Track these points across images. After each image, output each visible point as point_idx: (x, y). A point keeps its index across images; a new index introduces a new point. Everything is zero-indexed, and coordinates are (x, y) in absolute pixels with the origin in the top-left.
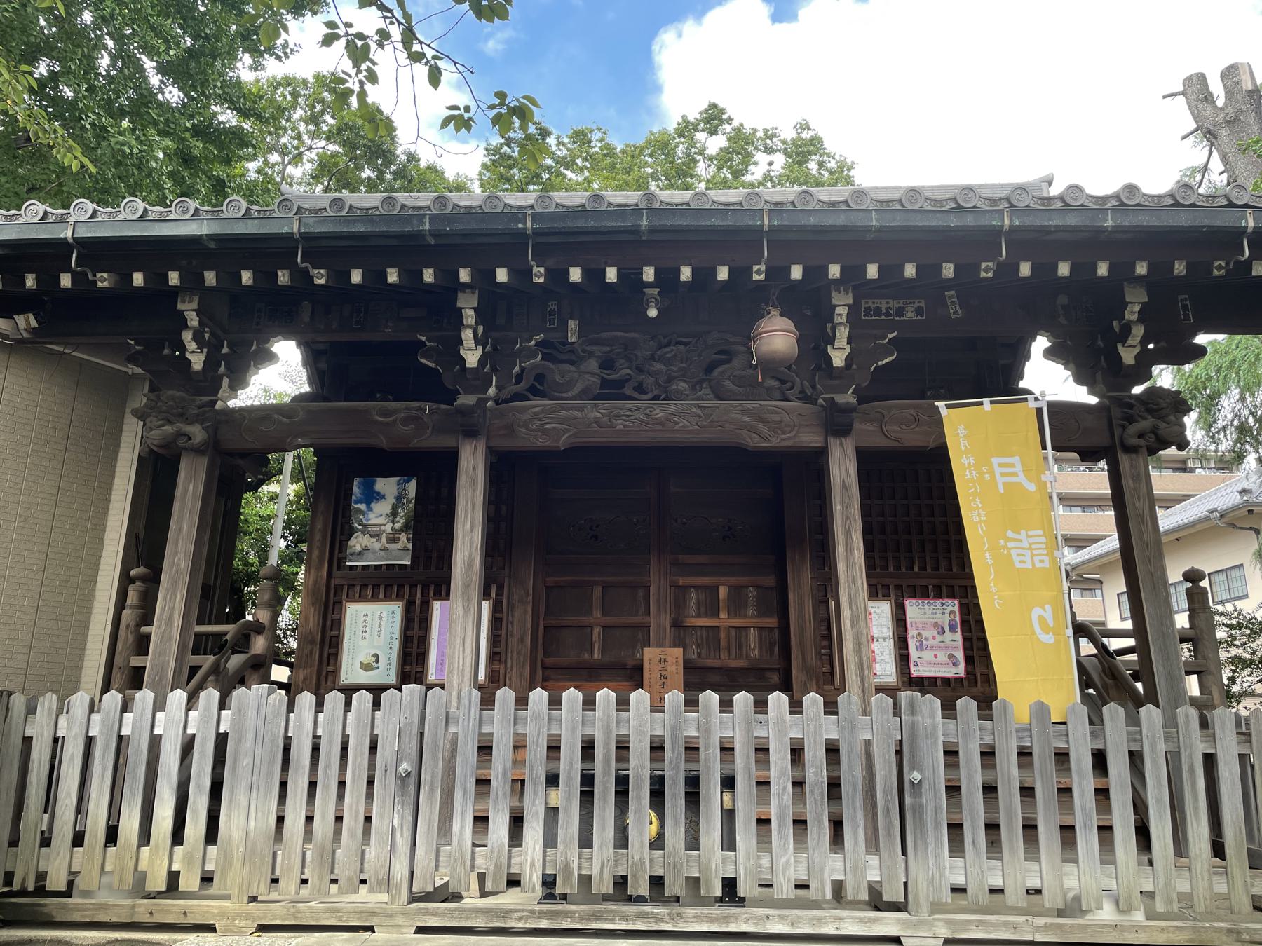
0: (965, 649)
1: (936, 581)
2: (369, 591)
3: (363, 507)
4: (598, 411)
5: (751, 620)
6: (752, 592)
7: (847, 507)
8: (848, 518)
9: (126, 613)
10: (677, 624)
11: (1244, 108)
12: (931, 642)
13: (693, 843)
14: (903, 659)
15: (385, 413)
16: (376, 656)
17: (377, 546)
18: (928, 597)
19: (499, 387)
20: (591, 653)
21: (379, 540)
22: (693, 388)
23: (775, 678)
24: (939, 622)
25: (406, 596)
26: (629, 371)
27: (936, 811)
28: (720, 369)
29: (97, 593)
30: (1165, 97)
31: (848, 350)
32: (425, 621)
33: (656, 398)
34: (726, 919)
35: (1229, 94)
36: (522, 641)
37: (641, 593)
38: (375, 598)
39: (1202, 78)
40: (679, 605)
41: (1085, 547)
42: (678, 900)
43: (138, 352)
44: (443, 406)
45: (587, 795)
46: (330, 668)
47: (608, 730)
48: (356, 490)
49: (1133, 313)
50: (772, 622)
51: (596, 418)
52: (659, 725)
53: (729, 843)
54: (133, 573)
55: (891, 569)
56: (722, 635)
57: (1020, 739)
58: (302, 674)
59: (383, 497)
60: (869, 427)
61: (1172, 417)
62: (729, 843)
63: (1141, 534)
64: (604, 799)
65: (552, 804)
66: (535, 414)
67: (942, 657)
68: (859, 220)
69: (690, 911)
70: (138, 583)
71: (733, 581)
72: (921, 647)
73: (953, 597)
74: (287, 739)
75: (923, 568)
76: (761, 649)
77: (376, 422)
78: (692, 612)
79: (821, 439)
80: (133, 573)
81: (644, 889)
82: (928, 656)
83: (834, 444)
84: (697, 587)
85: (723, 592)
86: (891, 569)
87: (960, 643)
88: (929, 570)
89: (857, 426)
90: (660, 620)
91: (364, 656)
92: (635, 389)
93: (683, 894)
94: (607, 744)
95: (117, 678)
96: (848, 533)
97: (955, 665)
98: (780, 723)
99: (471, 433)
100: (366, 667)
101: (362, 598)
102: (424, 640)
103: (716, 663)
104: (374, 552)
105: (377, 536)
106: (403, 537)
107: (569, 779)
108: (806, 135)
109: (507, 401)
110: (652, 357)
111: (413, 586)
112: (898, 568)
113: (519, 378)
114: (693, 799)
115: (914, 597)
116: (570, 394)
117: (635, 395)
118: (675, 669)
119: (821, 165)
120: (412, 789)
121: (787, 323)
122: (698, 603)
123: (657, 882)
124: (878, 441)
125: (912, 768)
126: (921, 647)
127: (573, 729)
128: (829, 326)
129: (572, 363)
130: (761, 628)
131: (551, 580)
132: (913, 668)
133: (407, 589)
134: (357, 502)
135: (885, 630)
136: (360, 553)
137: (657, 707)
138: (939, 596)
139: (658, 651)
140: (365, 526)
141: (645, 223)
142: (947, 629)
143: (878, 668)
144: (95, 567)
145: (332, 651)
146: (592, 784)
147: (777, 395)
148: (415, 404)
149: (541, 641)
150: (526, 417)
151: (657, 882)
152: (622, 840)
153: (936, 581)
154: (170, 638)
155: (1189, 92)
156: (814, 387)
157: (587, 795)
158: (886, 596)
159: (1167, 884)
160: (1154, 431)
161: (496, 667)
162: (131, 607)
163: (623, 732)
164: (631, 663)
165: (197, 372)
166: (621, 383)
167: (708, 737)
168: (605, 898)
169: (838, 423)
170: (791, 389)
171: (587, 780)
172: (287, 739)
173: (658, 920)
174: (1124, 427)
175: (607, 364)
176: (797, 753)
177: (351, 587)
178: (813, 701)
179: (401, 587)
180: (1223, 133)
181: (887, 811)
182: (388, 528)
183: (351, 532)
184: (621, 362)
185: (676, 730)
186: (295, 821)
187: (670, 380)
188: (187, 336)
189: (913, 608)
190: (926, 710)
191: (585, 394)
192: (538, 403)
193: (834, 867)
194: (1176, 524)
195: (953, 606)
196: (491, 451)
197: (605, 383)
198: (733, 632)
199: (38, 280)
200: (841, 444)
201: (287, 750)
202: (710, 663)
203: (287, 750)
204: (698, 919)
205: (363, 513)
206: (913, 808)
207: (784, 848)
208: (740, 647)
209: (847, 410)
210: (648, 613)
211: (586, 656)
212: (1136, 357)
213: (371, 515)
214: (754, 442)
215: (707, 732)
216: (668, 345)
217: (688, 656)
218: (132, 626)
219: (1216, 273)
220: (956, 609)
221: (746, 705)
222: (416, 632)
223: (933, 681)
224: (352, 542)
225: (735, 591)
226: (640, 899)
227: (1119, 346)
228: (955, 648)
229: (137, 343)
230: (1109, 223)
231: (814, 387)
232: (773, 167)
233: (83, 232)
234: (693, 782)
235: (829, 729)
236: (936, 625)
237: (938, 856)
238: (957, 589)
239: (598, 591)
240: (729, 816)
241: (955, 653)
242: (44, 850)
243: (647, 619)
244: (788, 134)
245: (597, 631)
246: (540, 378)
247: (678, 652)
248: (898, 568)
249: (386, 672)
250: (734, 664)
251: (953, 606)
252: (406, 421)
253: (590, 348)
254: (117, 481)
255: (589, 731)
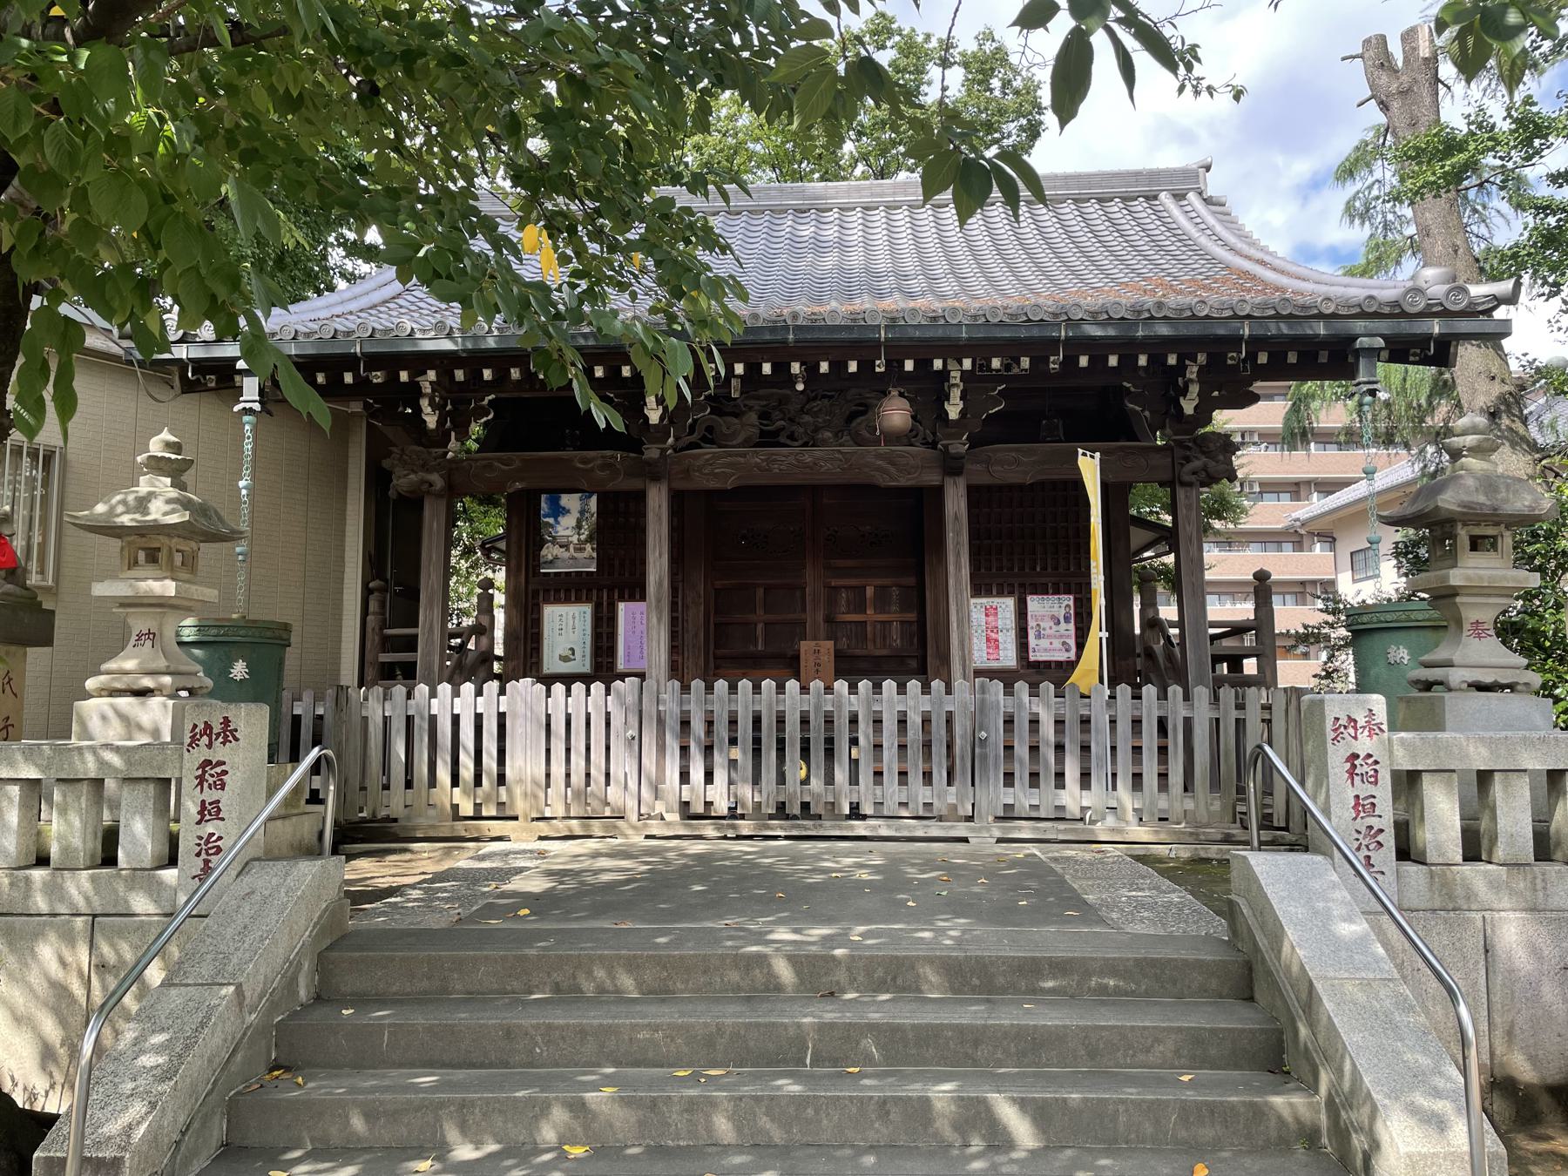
0: (1077, 637)
1: (1053, 579)
2: (562, 595)
3: (551, 520)
4: (759, 456)
5: (894, 616)
6: (895, 591)
7: (958, 534)
8: (958, 543)
9: (370, 618)
10: (829, 620)
11: (1419, 77)
12: (1048, 632)
13: (829, 779)
14: (1023, 646)
15: (585, 461)
16: (572, 650)
17: (566, 555)
18: (1047, 594)
19: (677, 439)
20: (756, 645)
21: (568, 550)
22: (836, 435)
23: (914, 664)
24: (1056, 614)
25: (594, 598)
26: (783, 422)
27: (997, 757)
28: (859, 420)
29: (345, 603)
30: (1344, 59)
31: (961, 406)
32: (612, 620)
33: (805, 444)
34: (852, 828)
35: (1406, 60)
36: (696, 635)
37: (798, 594)
38: (567, 601)
39: (1382, 40)
40: (832, 602)
41: (1334, 492)
42: (820, 817)
43: (378, 409)
44: (632, 455)
45: (757, 752)
46: (534, 660)
47: (770, 707)
48: (543, 505)
49: (1192, 373)
50: (912, 616)
51: (756, 463)
52: (808, 703)
53: (854, 780)
54: (371, 585)
55: (1016, 570)
56: (869, 628)
57: (1057, 709)
58: (511, 665)
59: (568, 511)
60: (979, 467)
61: (1221, 457)
62: (854, 780)
63: (1188, 552)
64: (769, 749)
65: (732, 757)
66: (708, 460)
67: (1057, 644)
68: (953, 334)
69: (827, 823)
70: (376, 594)
71: (879, 582)
72: (1038, 636)
73: (1069, 593)
74: (548, 716)
75: (1044, 568)
76: (902, 639)
77: (578, 469)
78: (843, 609)
79: (940, 478)
80: (371, 585)
81: (797, 811)
82: (1044, 643)
83: (949, 482)
84: (846, 588)
85: (870, 591)
86: (1016, 570)
87: (1073, 632)
88: (1049, 570)
89: (968, 466)
90: (815, 617)
91: (562, 649)
92: (788, 437)
93: (823, 813)
94: (770, 717)
95: (370, 673)
96: (958, 555)
97: (1067, 650)
98: (890, 700)
99: (656, 478)
100: (564, 659)
101: (557, 601)
102: (612, 636)
103: (864, 652)
104: (564, 560)
105: (565, 546)
106: (588, 547)
107: (744, 740)
108: (989, 47)
109: (683, 449)
110: (802, 409)
111: (600, 590)
112: (1022, 568)
113: (692, 428)
114: (830, 753)
115: (1036, 594)
116: (734, 443)
117: (789, 442)
118: (828, 659)
119: (1006, 84)
120: (636, 748)
121: (905, 403)
122: (848, 602)
123: (805, 806)
124: (984, 480)
125: (980, 731)
126: (1038, 636)
127: (746, 707)
128: (946, 384)
129: (736, 415)
130: (902, 622)
131: (718, 584)
132: (1031, 654)
133: (595, 592)
134: (545, 516)
135: (1008, 622)
136: (551, 562)
137: (805, 689)
138: (1057, 592)
139: (813, 643)
140: (554, 537)
141: (791, 337)
142: (1062, 620)
143: (976, 655)
144: (340, 581)
145: (535, 645)
146: (760, 744)
147: (905, 441)
148: (608, 453)
149: (712, 636)
150: (700, 462)
151: (805, 806)
152: (781, 779)
153: (1053, 579)
154: (433, 642)
155: (1366, 56)
156: (934, 434)
157: (757, 752)
158: (1010, 594)
159: (1152, 803)
160: (1205, 469)
161: (675, 658)
162: (374, 613)
163: (781, 708)
164: (790, 653)
165: (432, 430)
166: (777, 433)
167: (840, 711)
168: (771, 817)
169: (952, 466)
170: (916, 436)
171: (757, 741)
172: (548, 716)
173: (806, 829)
174: (1182, 465)
175: (764, 415)
176: (902, 722)
177: (547, 591)
178: (914, 685)
179: (589, 590)
180: (1395, 105)
181: (962, 758)
182: (575, 539)
183: (541, 544)
184: (776, 414)
185: (818, 707)
186: (558, 770)
187: (816, 430)
188: (424, 403)
189: (1034, 604)
190: (993, 690)
191: (746, 443)
192: (709, 451)
193: (923, 794)
194: (1395, 483)
195: (1069, 600)
196: (670, 489)
197: (763, 434)
198: (879, 626)
199: (327, 377)
200: (955, 483)
201: (548, 725)
202: (858, 652)
203: (548, 725)
204: (833, 827)
205: (552, 526)
206: (981, 755)
207: (892, 782)
208: (885, 638)
209: (959, 457)
210: (804, 610)
211: (752, 648)
212: (1196, 408)
213: (559, 528)
214: (884, 481)
215: (840, 707)
216: (815, 399)
217: (839, 647)
218: (377, 630)
219: (1229, 362)
220: (1071, 603)
221: (867, 689)
222: (605, 629)
223: (1048, 664)
224: (543, 552)
225: (881, 591)
226: (795, 817)
227: (1181, 399)
228: (1068, 637)
229: (375, 402)
230: (1140, 333)
231: (934, 434)
232: (947, 93)
233: (369, 349)
234: (830, 741)
235: (925, 703)
236: (1053, 617)
237: (996, 786)
238: (1073, 586)
239: (760, 592)
240: (854, 764)
241: (1068, 641)
242: (385, 792)
243: (803, 616)
244: (966, 43)
245: (760, 627)
246: (710, 429)
247: (830, 644)
248: (1022, 568)
249: (583, 664)
250: (878, 653)
251: (1069, 600)
252: (603, 467)
253: (751, 403)
254: (349, 507)
255: (757, 708)
